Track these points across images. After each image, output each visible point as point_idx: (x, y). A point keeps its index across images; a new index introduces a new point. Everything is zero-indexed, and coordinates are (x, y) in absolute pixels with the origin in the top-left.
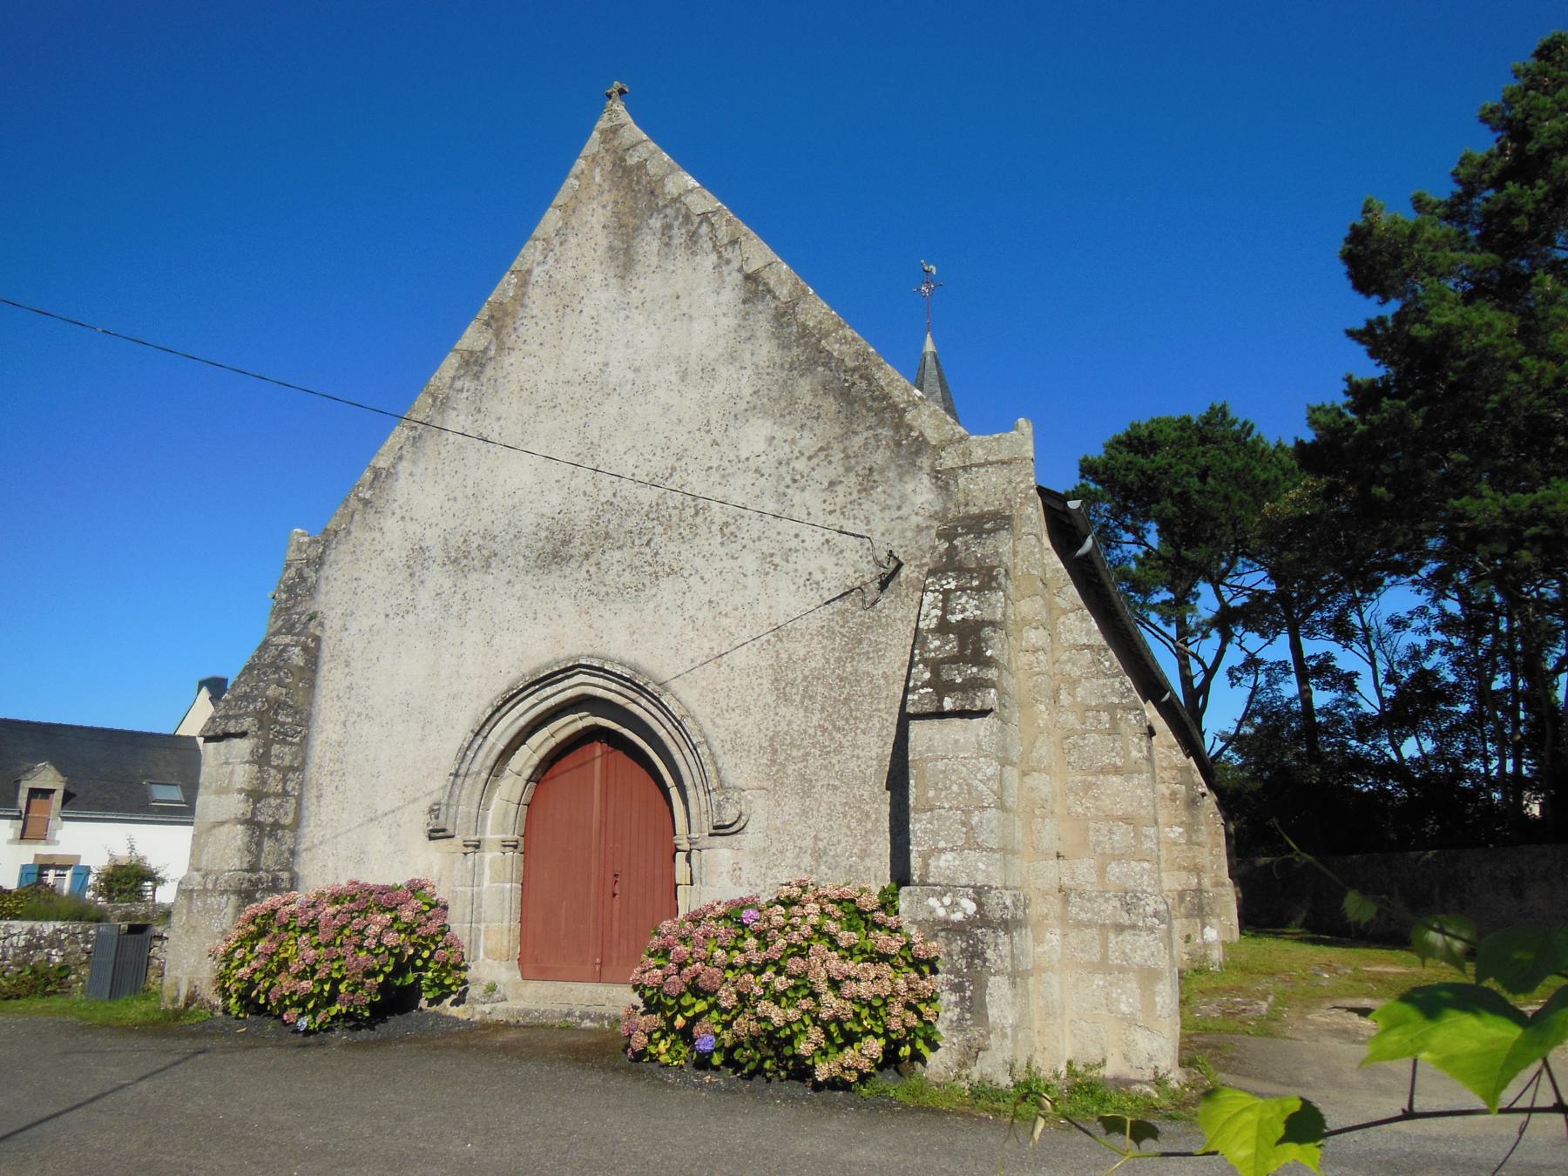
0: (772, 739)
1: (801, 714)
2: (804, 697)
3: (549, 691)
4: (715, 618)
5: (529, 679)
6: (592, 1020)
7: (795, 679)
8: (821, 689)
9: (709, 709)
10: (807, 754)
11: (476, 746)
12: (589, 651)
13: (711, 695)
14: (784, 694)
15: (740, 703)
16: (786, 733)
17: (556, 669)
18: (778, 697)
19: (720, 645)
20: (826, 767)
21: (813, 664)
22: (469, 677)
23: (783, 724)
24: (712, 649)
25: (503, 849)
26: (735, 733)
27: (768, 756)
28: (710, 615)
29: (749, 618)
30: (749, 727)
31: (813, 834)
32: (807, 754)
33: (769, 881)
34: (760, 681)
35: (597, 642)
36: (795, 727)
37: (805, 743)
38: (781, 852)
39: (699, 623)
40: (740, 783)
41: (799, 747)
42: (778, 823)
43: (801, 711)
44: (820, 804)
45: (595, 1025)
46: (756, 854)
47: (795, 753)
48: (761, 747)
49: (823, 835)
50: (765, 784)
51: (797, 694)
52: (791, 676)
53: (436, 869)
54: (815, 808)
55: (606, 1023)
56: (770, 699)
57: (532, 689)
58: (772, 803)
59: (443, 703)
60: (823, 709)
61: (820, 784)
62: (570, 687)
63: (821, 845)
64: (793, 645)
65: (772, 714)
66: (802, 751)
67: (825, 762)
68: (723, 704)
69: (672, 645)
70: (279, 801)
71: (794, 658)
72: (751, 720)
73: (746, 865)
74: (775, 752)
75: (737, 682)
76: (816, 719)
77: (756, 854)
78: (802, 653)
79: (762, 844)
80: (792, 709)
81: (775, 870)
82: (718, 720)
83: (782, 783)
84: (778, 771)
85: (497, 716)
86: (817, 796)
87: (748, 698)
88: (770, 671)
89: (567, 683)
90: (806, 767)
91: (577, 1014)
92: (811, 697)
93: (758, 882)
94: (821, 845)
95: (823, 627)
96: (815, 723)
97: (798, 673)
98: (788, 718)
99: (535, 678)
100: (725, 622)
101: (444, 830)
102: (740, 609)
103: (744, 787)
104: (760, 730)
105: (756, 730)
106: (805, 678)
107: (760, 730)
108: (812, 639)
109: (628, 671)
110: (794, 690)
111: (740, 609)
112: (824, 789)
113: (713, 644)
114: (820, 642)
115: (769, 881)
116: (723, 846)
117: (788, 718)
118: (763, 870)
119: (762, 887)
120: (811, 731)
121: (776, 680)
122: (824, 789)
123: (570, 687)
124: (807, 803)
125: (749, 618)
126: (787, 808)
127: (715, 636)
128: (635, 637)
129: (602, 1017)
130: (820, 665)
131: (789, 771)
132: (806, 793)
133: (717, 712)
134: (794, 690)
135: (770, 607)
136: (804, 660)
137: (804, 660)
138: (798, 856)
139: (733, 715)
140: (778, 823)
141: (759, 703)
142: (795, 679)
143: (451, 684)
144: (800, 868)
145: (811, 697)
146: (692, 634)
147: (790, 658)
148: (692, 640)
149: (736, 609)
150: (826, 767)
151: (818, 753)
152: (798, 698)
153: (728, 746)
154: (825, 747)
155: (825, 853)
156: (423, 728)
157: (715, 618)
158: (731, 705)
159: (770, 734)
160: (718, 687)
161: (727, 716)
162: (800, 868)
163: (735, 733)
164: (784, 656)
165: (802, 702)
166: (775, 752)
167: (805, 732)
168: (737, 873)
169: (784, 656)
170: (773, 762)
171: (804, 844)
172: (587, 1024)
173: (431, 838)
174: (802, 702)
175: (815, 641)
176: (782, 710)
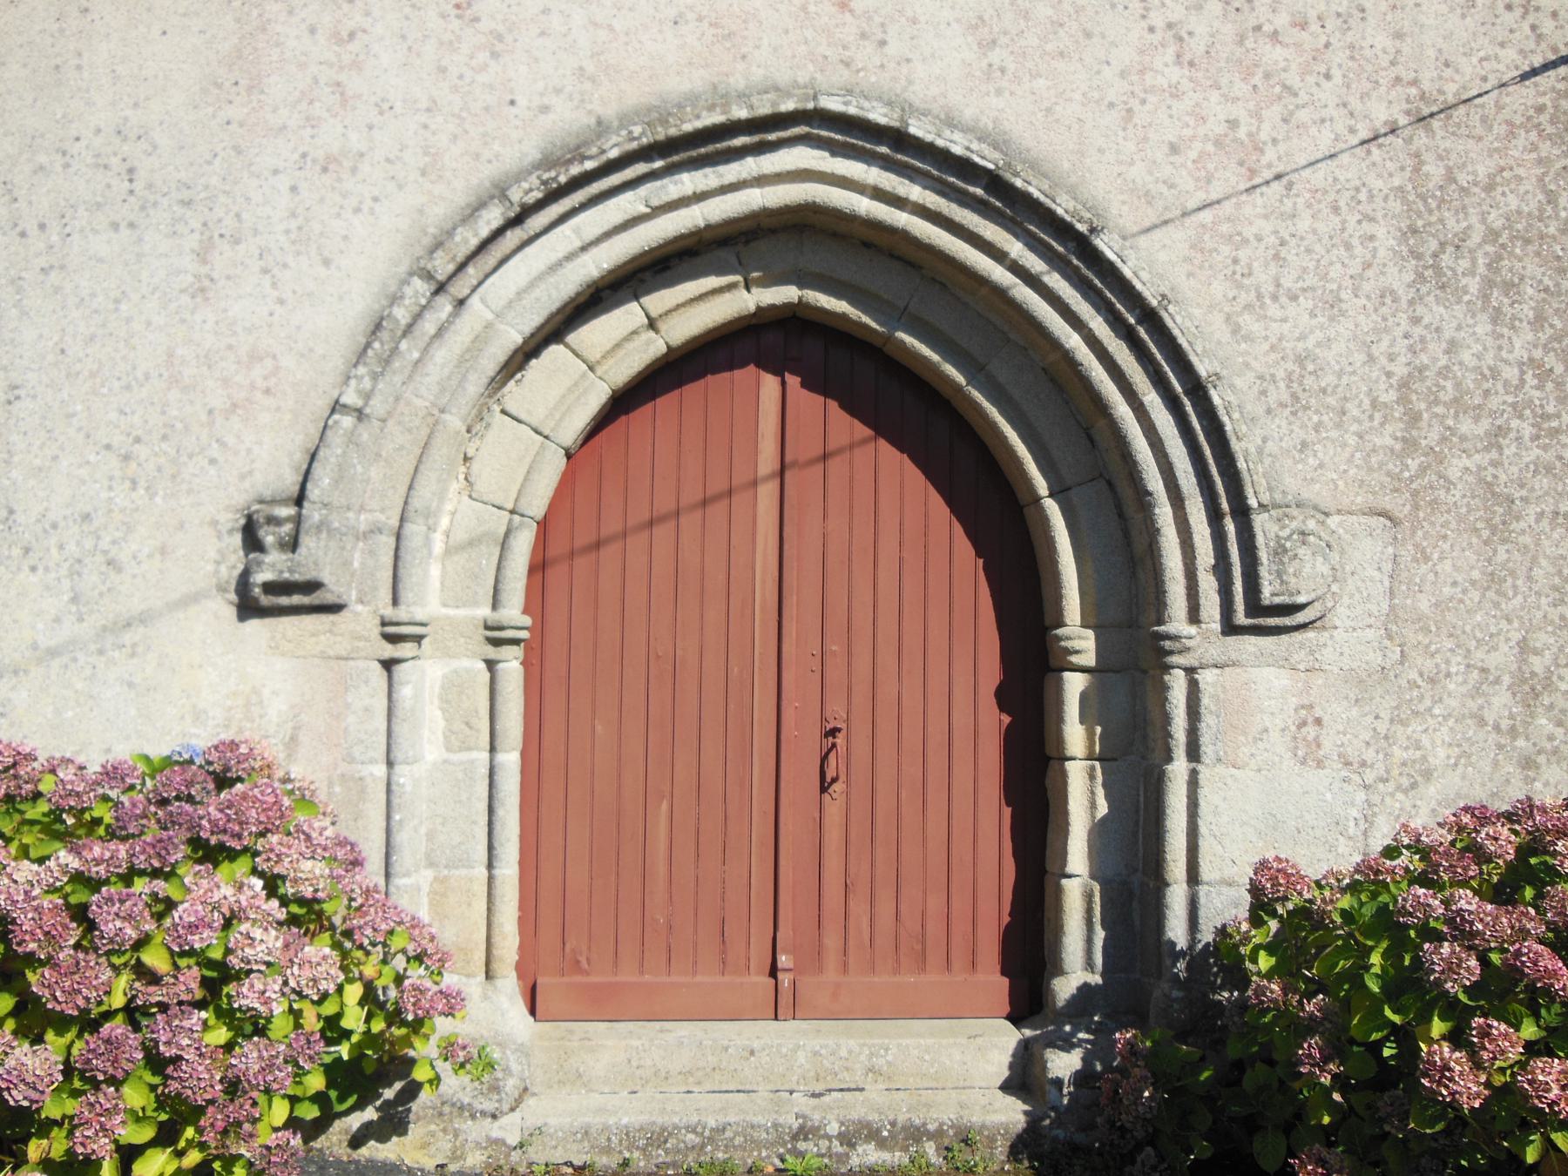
0: (1404, 385)
1: (1483, 327)
2: (1489, 283)
3: (688, 182)
4: (1241, 40)
5: (643, 135)
6: (882, 1144)
7: (1464, 235)
8: (1532, 268)
9: (1219, 288)
10: (1501, 431)
11: (429, 326)
12: (842, 76)
13: (1226, 250)
14: (1436, 268)
15: (1310, 280)
16: (1444, 372)
17: (742, 113)
18: (1420, 277)
19: (1257, 115)
20: (1549, 469)
21: (1513, 202)
22: (384, 107)
23: (1436, 348)
24: (1233, 124)
25: (492, 652)
26: (1300, 360)
27: (1392, 428)
28: (1229, 30)
29: (1339, 57)
30: (1339, 347)
31: (1516, 636)
32: (1501, 431)
33: (1398, 754)
34: (1367, 227)
35: (865, 55)
36: (1466, 356)
37: (1494, 403)
38: (1432, 681)
39: (1197, 46)
40: (1316, 493)
41: (1477, 412)
42: (1424, 604)
43: (1484, 318)
44: (1534, 560)
45: (897, 1158)
46: (1361, 684)
47: (1466, 427)
48: (1374, 404)
49: (1541, 639)
50: (1387, 502)
51: (1471, 272)
52: (1453, 225)
53: (276, 709)
54: (1522, 572)
55: (930, 1148)
56: (1399, 278)
57: (641, 168)
58: (1407, 553)
59: (284, 182)
60: (1539, 321)
61: (1533, 510)
62: (761, 181)
63: (1537, 664)
64: (1460, 145)
65: (1403, 318)
66: (1485, 424)
67: (1549, 456)
68: (1263, 278)
69: (1111, 96)
70: (1430, 200)
71: (1463, 179)
72: (1344, 328)
73: (1337, 712)
74: (1414, 418)
75: (1304, 224)
76: (1521, 344)
77: (1361, 684)
78: (1482, 170)
79: (1376, 659)
80: (1459, 310)
81: (1415, 727)
82: (1248, 322)
83: (1435, 502)
84: (1423, 470)
85: (513, 237)
86: (1526, 539)
87: (1335, 272)
88: (1396, 206)
89: (750, 166)
90: (1495, 464)
91: (833, 1128)
92: (1508, 287)
93: (1369, 755)
94: (1537, 664)
95: (1540, 109)
96: (1520, 352)
97: (1474, 219)
98: (1447, 335)
99: (661, 134)
100: (1274, 55)
101: (312, 586)
102: (1314, 27)
103: (1327, 503)
104: (1371, 359)
105: (1359, 358)
106: (1492, 235)
107: (1371, 359)
108: (1511, 135)
109: (985, 149)
110: (1464, 264)
111: (1314, 27)
112: (1545, 523)
113: (1238, 111)
114: (1534, 148)
115: (1398, 754)
116: (1262, 659)
117: (1447, 335)
118: (1382, 727)
119: (1380, 769)
120: (1511, 373)
121: (1414, 231)
122: (1545, 523)
123: (761, 181)
124: (1502, 556)
125: (1339, 57)
126: (1447, 566)
127: (1241, 89)
128: (995, 56)
129: (916, 1134)
130: (1531, 206)
131: (1454, 473)
132: (1499, 532)
133: (1244, 298)
134: (1464, 264)
135: (1399, 35)
136: (1490, 188)
137: (1490, 188)
138: (1477, 691)
139: (1292, 310)
140: (1424, 604)
141: (1367, 287)
142: (1464, 235)
143: (311, 122)
144: (1482, 722)
145: (1508, 287)
146: (1175, 74)
147: (1450, 178)
148: (1175, 93)
149: (1303, 26)
150: (1549, 469)
151: (1528, 431)
152: (1473, 285)
153: (1279, 393)
154: (1546, 417)
155: (1548, 685)
156: (202, 255)
157: (1241, 40)
158: (1287, 282)
159: (1400, 370)
160: (1249, 232)
161: (1273, 310)
162: (1482, 722)
163: (1300, 360)
164: (1435, 170)
165: (1486, 298)
166: (1414, 418)
167: (1495, 373)
168: (1311, 731)
169: (1435, 170)
170: (1410, 445)
171: (1494, 660)
172: (868, 1154)
173: (248, 608)
174: (1486, 298)
175: (1522, 140)
176: (1433, 312)
